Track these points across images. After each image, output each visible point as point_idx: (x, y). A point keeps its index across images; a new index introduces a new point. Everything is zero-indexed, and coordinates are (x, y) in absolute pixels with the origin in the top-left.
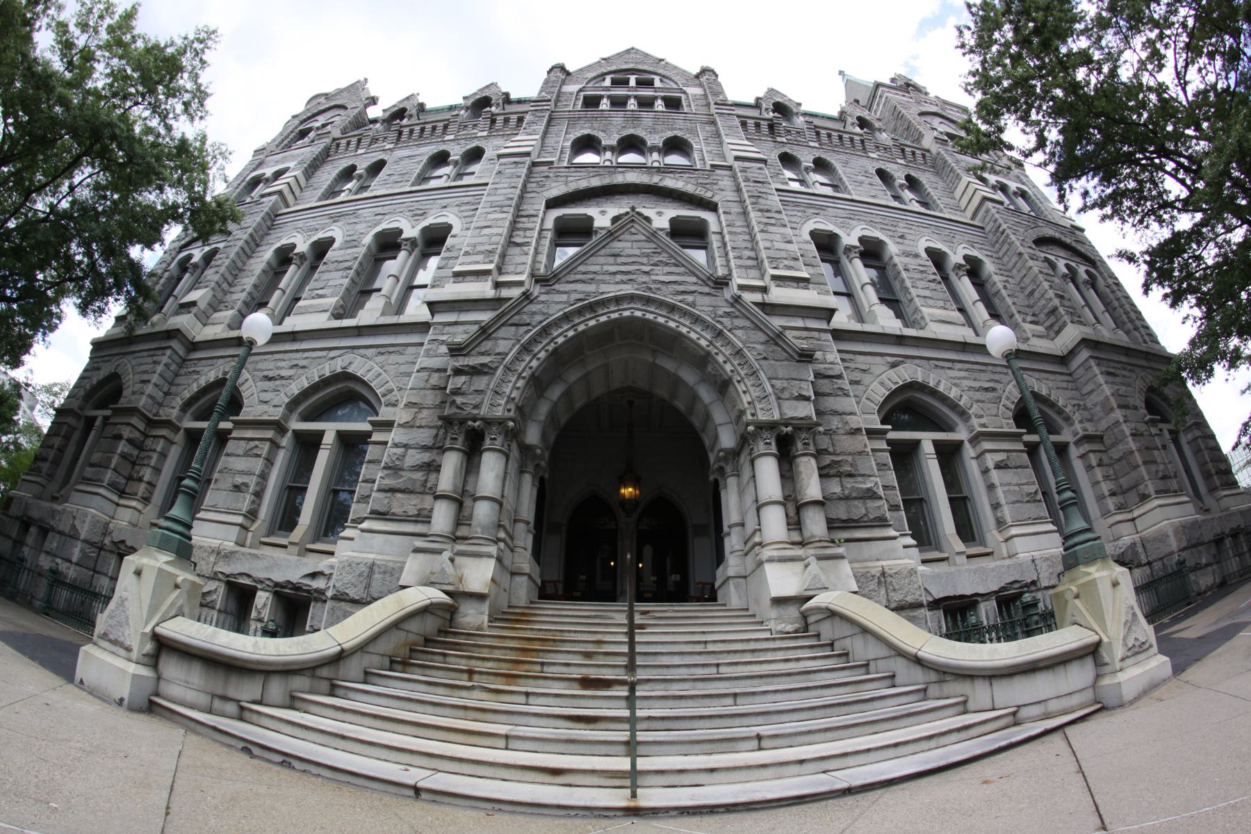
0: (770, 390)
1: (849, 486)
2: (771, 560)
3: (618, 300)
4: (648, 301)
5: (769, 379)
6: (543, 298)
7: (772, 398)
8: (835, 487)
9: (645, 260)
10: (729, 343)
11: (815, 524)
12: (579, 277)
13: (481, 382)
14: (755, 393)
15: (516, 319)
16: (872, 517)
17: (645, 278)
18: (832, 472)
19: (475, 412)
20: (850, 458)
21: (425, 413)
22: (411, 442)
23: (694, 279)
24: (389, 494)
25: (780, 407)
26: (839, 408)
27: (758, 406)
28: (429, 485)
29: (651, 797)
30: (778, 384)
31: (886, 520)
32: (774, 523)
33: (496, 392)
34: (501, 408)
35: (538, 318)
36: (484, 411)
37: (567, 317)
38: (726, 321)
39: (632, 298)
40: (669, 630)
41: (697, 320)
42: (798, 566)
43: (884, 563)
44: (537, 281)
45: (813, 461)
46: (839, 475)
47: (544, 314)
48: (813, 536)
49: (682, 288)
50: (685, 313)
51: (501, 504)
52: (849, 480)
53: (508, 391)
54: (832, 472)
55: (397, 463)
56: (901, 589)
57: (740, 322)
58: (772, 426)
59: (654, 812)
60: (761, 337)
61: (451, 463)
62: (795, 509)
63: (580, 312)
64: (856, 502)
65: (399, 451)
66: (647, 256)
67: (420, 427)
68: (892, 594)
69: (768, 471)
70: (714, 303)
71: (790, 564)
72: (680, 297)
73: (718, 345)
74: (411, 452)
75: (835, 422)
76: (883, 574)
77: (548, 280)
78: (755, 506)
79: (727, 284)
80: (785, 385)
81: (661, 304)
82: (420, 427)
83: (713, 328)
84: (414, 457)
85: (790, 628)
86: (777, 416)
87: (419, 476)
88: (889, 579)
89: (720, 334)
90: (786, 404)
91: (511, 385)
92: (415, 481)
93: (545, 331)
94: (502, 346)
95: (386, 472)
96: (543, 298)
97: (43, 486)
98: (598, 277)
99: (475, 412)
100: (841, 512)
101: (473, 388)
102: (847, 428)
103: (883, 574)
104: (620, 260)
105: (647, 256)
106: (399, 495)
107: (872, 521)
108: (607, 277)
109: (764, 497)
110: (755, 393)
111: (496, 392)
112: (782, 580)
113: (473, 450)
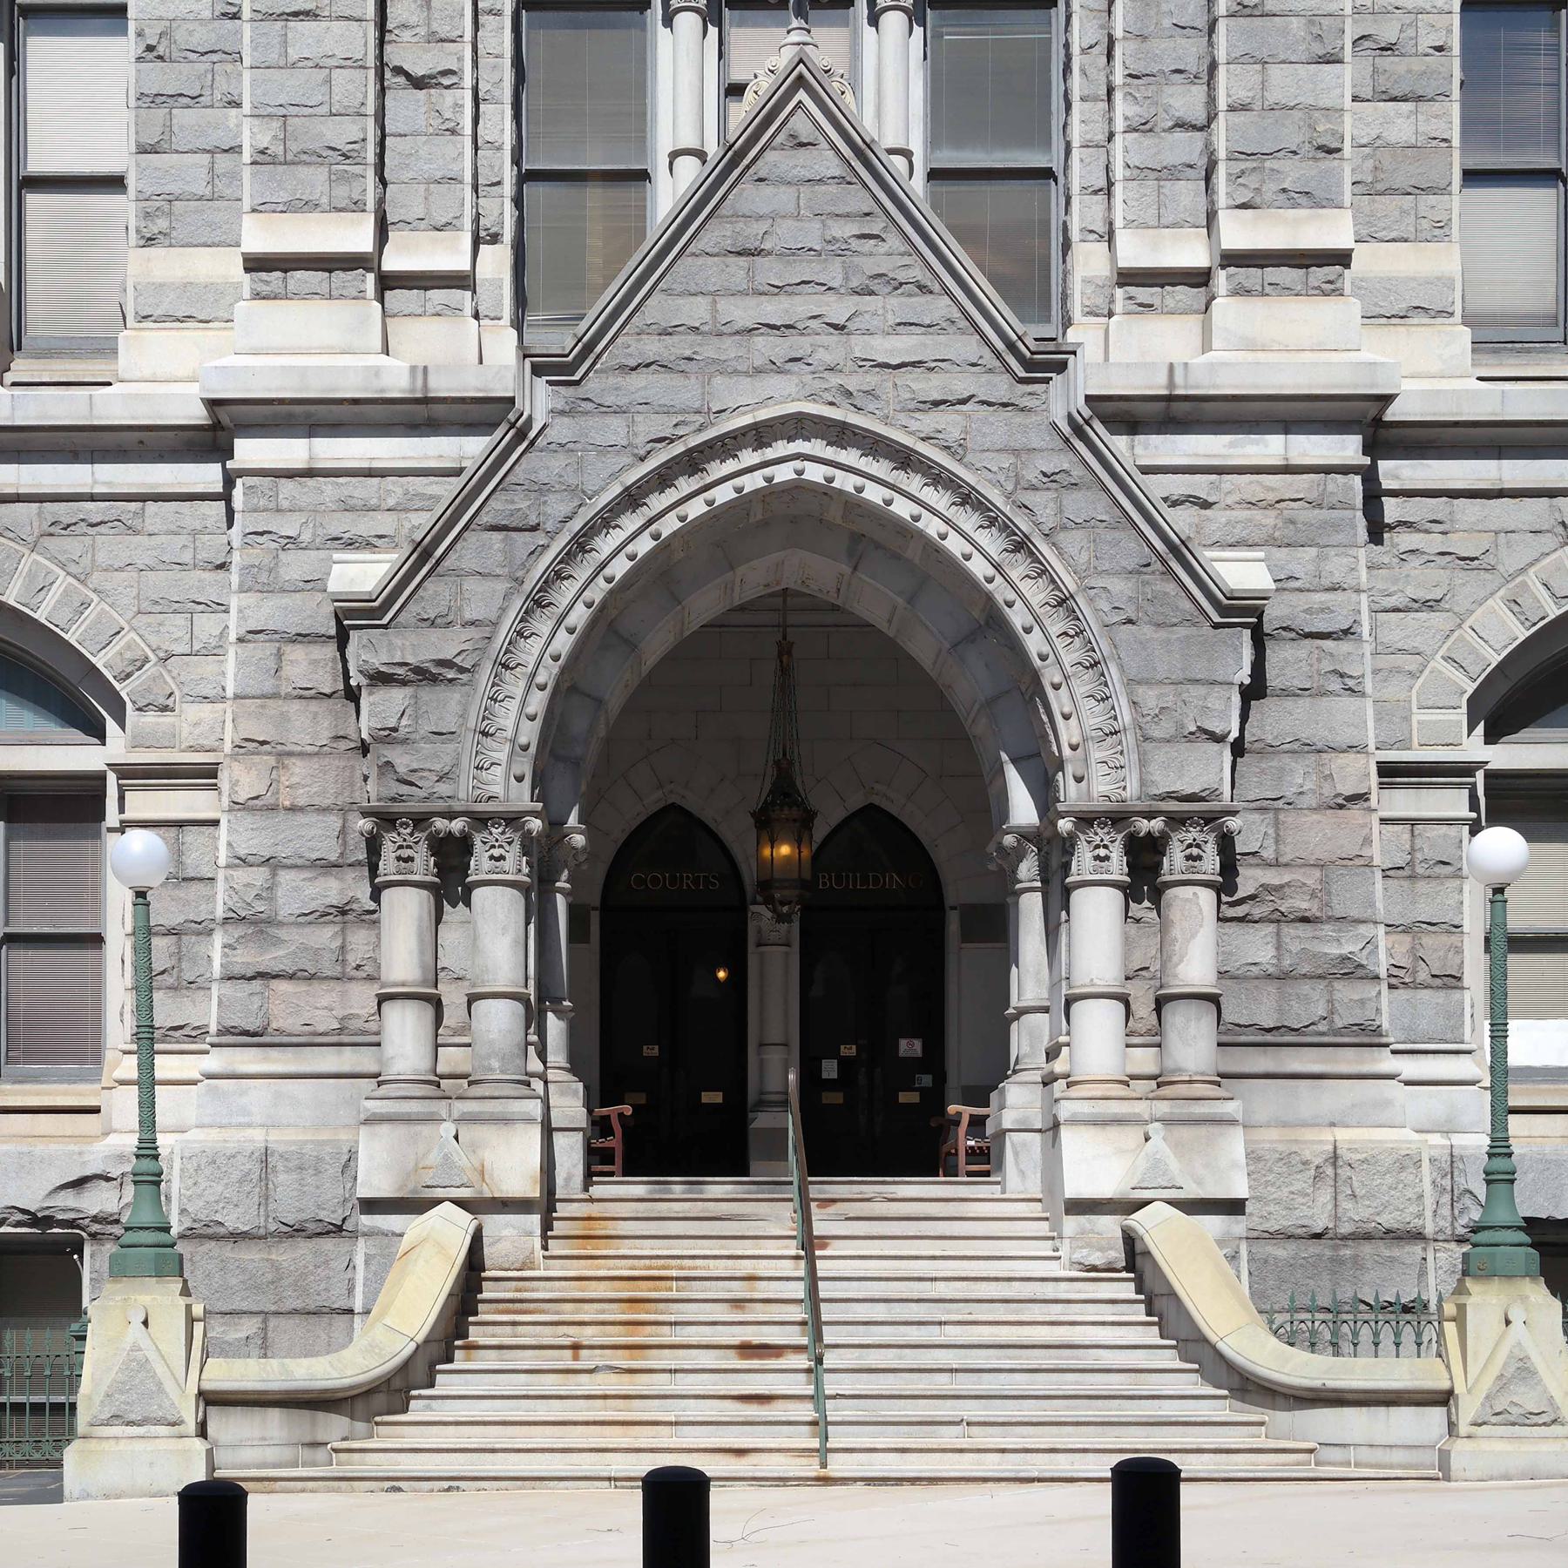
0: (1126, 716)
1: (1295, 947)
2: (1074, 1122)
3: (760, 434)
4: (841, 434)
5: (1131, 683)
6: (562, 431)
7: (1129, 740)
8: (1257, 947)
9: (833, 273)
10: (1043, 571)
11: (1192, 1043)
12: (652, 348)
13: (445, 707)
14: (1093, 715)
15: (498, 509)
16: (1339, 1023)
17: (829, 349)
18: (1258, 911)
19: (444, 789)
20: (1312, 878)
21: (298, 770)
22: (282, 852)
23: (969, 347)
24: (257, 985)
25: (1143, 763)
26: (1320, 735)
27: (1097, 754)
28: (353, 959)
29: (839, 1465)
30: (1150, 698)
31: (1377, 1031)
32: (1098, 1038)
33: (485, 734)
34: (498, 771)
35: (557, 506)
36: (463, 792)
37: (632, 499)
38: (1042, 503)
39: (798, 426)
40: (883, 1231)
41: (968, 498)
42: (1133, 1135)
43: (1342, 1135)
44: (537, 371)
45: (1206, 897)
46: (1278, 918)
47: (572, 490)
48: (1179, 1070)
49: (931, 386)
50: (939, 478)
51: (437, 1003)
52: (1303, 930)
53: (509, 723)
54: (1258, 911)
55: (260, 906)
56: (1370, 1196)
57: (1082, 504)
58: (1117, 818)
59: (844, 1481)
60: (1130, 551)
61: (405, 909)
62: (1152, 1005)
63: (662, 479)
64: (1305, 988)
65: (259, 876)
66: (842, 252)
67: (293, 809)
68: (1346, 1204)
69: (1097, 913)
70: (1019, 441)
71: (1113, 1132)
72: (929, 421)
73: (1014, 575)
74: (285, 877)
75: (1299, 777)
76: (1335, 1158)
77: (571, 368)
78: (1264, 53)
79: (1061, 367)
80: (1169, 701)
81: (875, 445)
82: (293, 809)
83: (1007, 528)
84: (300, 893)
85: (1097, 1259)
86: (1132, 790)
87: (325, 936)
88: (1344, 1172)
89: (1021, 545)
90: (1160, 755)
91: (513, 706)
92: (317, 951)
93: (580, 545)
94: (480, 599)
95: (239, 931)
96: (562, 431)
97: (1159, 1046)
98: (709, 350)
99: (444, 789)
100: (1263, 1010)
101: (426, 727)
102: (1328, 791)
103: (1335, 1158)
104: (770, 271)
105: (842, 252)
106: (282, 986)
107: (1337, 1032)
108: (729, 349)
109: (1081, 983)
110: (1093, 715)
111: (485, 734)
112: (1095, 1164)
113: (451, 881)
